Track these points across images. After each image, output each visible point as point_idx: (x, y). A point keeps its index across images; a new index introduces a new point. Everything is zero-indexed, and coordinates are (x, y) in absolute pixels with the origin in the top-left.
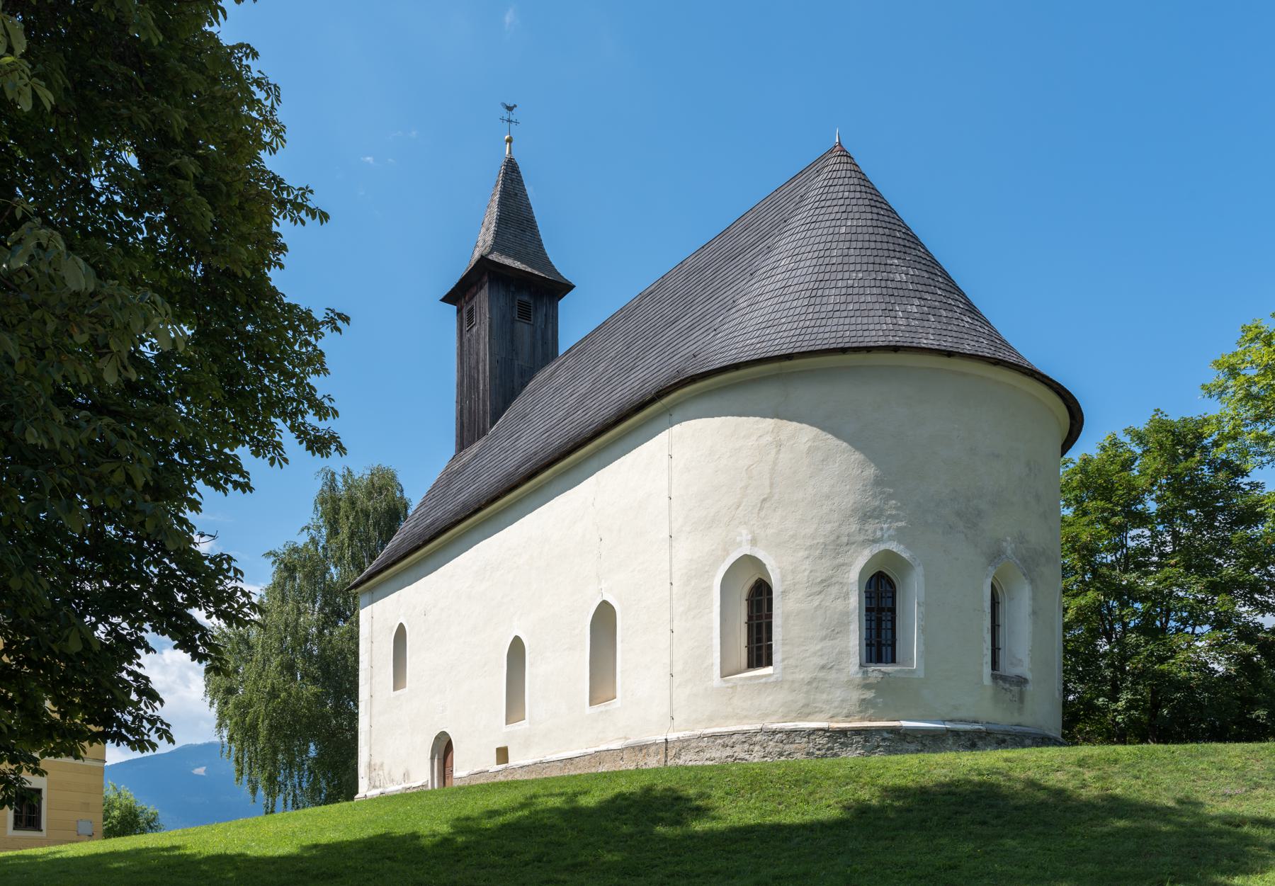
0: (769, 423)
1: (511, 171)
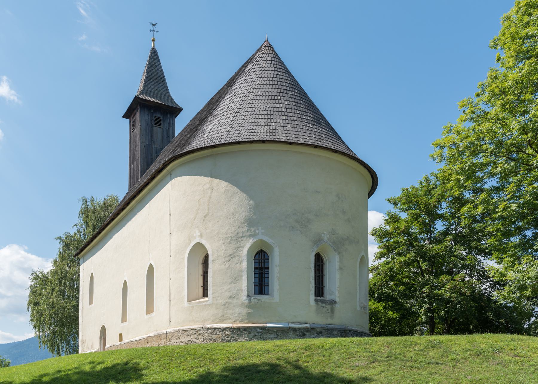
0: (207, 179)
1: (154, 54)
